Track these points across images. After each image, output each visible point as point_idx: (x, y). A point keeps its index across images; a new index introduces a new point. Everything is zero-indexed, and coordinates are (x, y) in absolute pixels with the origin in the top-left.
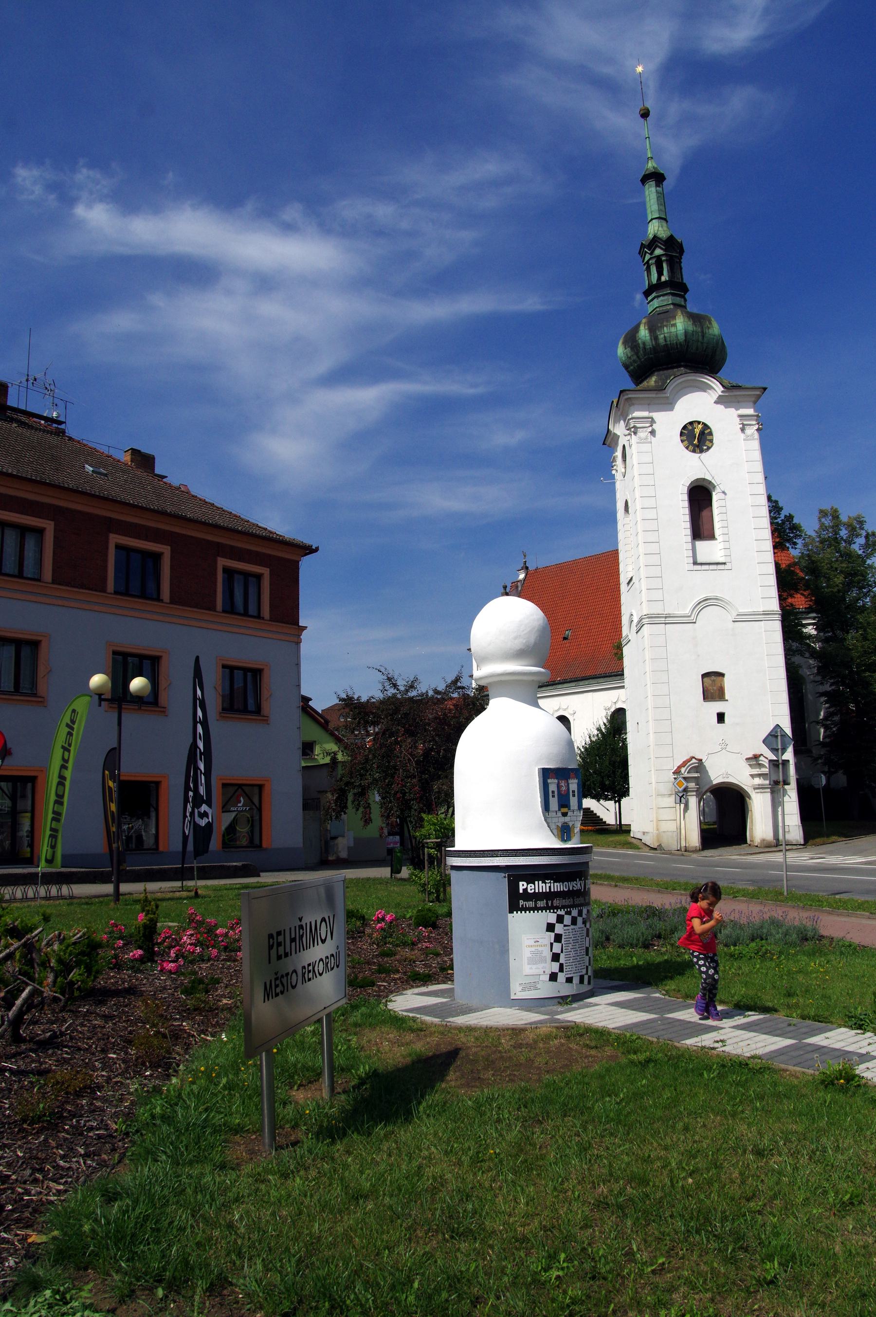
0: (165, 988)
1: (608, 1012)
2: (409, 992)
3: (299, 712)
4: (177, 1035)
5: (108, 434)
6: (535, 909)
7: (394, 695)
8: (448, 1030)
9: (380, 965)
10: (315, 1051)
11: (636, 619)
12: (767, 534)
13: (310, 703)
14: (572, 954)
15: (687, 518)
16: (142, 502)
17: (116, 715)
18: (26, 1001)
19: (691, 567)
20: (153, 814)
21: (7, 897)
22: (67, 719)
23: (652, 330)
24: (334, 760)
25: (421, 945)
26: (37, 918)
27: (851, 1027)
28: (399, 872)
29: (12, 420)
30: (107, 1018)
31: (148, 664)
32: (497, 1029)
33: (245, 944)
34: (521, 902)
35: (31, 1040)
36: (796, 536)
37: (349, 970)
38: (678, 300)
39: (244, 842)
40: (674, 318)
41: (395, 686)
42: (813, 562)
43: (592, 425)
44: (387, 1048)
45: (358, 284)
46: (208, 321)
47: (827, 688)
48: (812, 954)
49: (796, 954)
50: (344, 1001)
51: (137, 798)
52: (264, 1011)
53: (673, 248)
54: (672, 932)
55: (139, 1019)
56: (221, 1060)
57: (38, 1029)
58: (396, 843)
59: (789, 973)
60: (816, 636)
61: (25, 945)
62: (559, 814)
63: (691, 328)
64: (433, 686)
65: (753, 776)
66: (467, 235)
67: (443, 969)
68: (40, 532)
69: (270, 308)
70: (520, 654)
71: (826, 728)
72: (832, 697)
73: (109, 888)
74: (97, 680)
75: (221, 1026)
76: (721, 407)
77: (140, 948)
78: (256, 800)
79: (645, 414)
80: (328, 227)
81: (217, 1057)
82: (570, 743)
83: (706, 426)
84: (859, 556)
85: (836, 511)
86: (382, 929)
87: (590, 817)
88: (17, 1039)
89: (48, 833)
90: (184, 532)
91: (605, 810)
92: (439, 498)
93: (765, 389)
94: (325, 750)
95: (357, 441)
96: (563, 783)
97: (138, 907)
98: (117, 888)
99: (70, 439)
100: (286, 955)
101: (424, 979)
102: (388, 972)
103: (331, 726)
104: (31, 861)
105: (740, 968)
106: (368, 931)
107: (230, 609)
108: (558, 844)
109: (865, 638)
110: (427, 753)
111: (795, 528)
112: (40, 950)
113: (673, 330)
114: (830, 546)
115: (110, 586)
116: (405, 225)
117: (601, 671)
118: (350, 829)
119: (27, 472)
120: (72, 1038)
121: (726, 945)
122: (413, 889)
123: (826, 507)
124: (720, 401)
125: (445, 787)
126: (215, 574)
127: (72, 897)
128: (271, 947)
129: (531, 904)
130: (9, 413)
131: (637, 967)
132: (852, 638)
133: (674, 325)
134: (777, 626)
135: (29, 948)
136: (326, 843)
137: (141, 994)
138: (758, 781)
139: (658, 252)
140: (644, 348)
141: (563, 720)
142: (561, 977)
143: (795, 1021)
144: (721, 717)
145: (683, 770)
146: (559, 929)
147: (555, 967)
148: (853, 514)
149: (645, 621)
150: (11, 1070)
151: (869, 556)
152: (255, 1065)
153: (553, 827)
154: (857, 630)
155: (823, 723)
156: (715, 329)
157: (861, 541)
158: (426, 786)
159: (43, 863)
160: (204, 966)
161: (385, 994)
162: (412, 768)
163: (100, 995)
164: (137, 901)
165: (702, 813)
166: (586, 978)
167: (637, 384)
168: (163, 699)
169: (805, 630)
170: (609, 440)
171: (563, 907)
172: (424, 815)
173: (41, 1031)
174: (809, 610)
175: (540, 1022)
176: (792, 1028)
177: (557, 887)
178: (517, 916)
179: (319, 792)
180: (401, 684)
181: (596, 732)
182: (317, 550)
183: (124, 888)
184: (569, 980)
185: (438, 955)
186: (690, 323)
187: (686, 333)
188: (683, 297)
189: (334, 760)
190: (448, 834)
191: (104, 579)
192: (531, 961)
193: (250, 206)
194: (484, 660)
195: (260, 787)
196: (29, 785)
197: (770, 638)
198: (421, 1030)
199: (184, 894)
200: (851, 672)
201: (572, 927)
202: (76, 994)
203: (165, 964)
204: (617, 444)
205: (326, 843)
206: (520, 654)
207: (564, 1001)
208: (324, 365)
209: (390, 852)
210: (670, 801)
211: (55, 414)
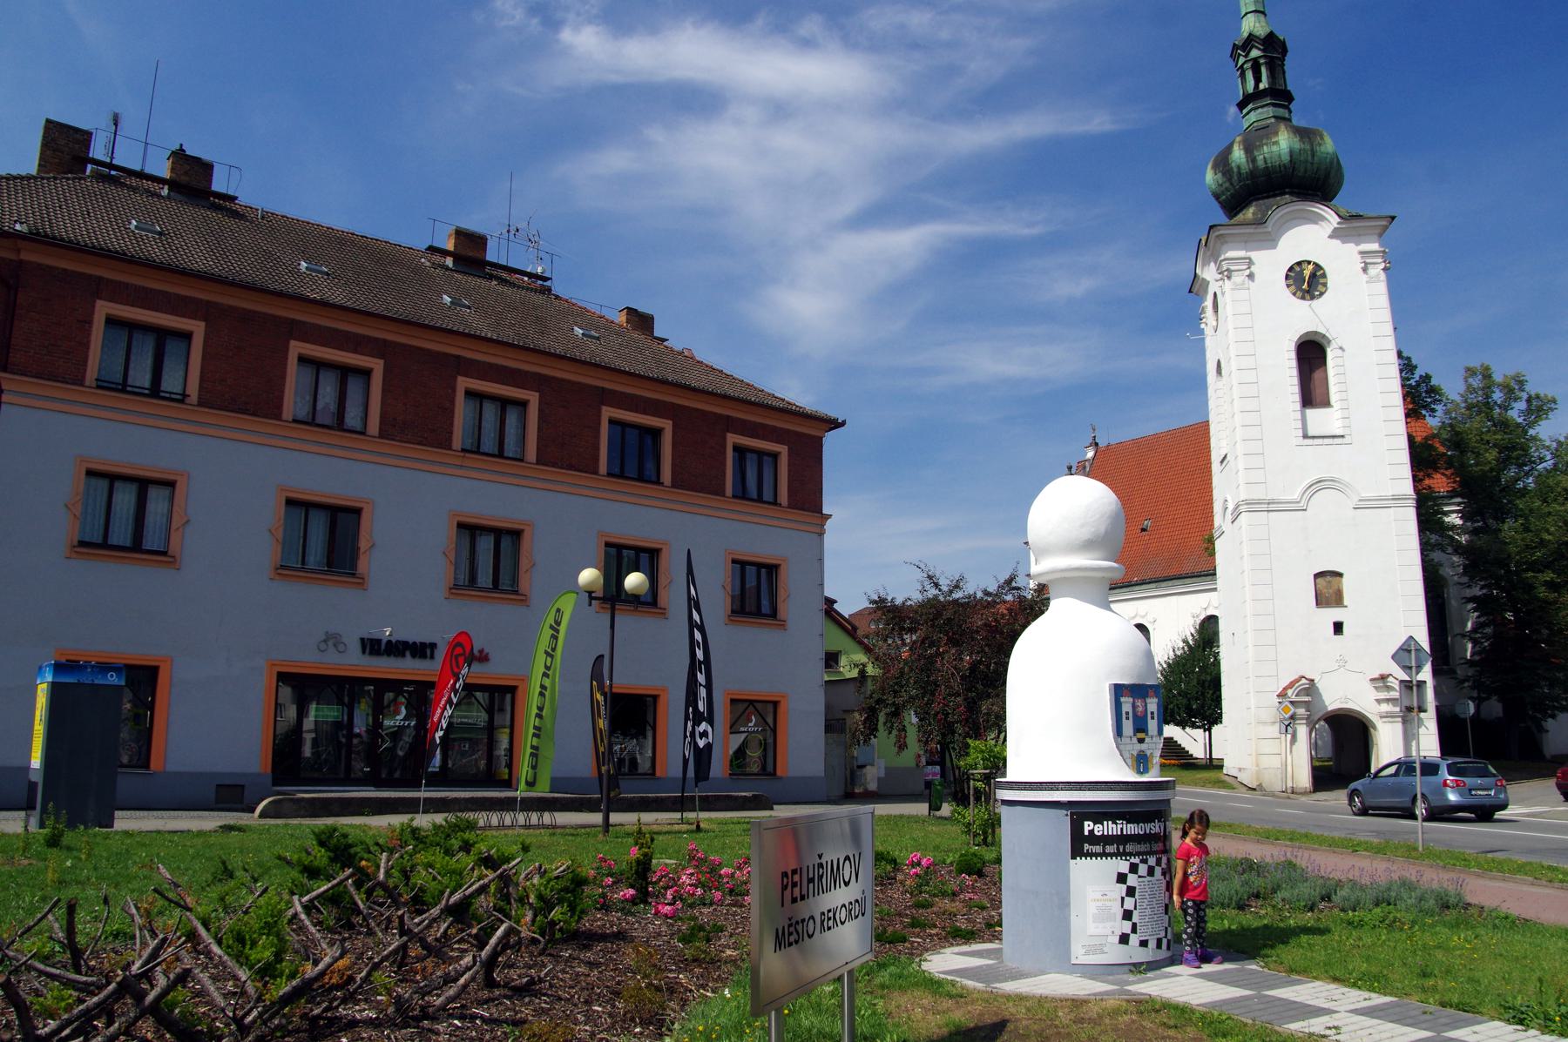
0: (659, 934)
1: (1190, 986)
2: (948, 950)
3: (821, 615)
4: (672, 989)
5: (597, 290)
6: (1104, 855)
7: (936, 596)
8: (993, 997)
9: (913, 918)
10: (834, 1015)
11: (1231, 506)
12: (1397, 399)
13: (836, 606)
14: (1148, 911)
15: (1296, 381)
16: (640, 369)
17: (607, 617)
18: (500, 940)
19: (1301, 441)
20: (650, 734)
21: (481, 823)
22: (550, 620)
23: (1249, 149)
24: (862, 673)
25: (961, 897)
26: (515, 848)
27: (1508, 1021)
28: (939, 809)
29: (491, 277)
30: (592, 965)
31: (647, 558)
32: (1054, 999)
33: (754, 887)
34: (1086, 847)
35: (506, 986)
36: (1435, 401)
37: (876, 923)
38: (1282, 112)
39: (755, 769)
40: (1276, 133)
41: (936, 585)
42: (1457, 434)
43: (1175, 268)
44: (920, 1016)
45: (887, 107)
46: (713, 156)
47: (1476, 591)
48: (1455, 926)
49: (1433, 926)
50: (870, 956)
51: (630, 714)
52: (774, 964)
53: (1274, 47)
54: (1274, 891)
55: (628, 969)
56: (722, 1020)
57: (514, 974)
58: (935, 774)
59: (1425, 946)
60: (1461, 527)
61: (501, 877)
62: (1135, 740)
63: (1297, 145)
64: (982, 586)
65: (1379, 701)
66: (1019, 45)
67: (989, 925)
68: (523, 404)
69: (786, 139)
70: (1088, 545)
71: (1475, 642)
72: (1482, 604)
73: (596, 818)
74: (588, 575)
75: (723, 981)
76: (1336, 242)
77: (632, 887)
78: (770, 720)
79: (1242, 253)
80: (851, 42)
81: (717, 1016)
82: (1149, 655)
83: (1318, 267)
84: (1518, 425)
85: (1487, 368)
86: (916, 874)
87: (1172, 750)
88: (490, 983)
89: (529, 751)
90: (687, 403)
91: (1192, 740)
92: (991, 361)
93: (1393, 218)
94: (852, 662)
95: (894, 293)
96: (1139, 703)
97: (631, 840)
98: (606, 818)
99: (557, 297)
100: (803, 898)
101: (968, 936)
102: (923, 926)
103: (860, 633)
104: (508, 784)
105: (1360, 939)
106: (900, 877)
107: (742, 494)
108: (1132, 777)
109: (1527, 529)
110: (974, 667)
111: (1433, 391)
112: (517, 884)
113: (1275, 148)
114: (1479, 413)
115: (603, 467)
116: (945, 35)
117: (1186, 570)
118: (883, 755)
119: (509, 335)
120: (551, 986)
121: (1343, 910)
122: (956, 829)
123: (1475, 363)
124: (1335, 234)
125: (995, 708)
126: (724, 453)
127: (555, 827)
128: (784, 888)
129: (1098, 849)
130: (488, 269)
131: (1229, 932)
132: (1509, 528)
133: (1276, 143)
134: (1411, 513)
135: (505, 880)
136: (853, 773)
137: (632, 939)
138: (1385, 707)
139: (1255, 53)
140: (1239, 173)
141: (1141, 628)
142: (1134, 940)
143: (1432, 1008)
144: (1338, 628)
145: (1290, 692)
146: (1132, 880)
147: (1127, 929)
148: (1511, 373)
149: (1242, 508)
150: (482, 1017)
151: (1531, 425)
152: (763, 1028)
153: (1127, 755)
154: (1516, 518)
155: (1470, 636)
156: (1328, 145)
157: (1522, 405)
158: (972, 706)
159: (522, 785)
160: (705, 910)
161: (918, 952)
162: (956, 683)
163: (585, 939)
164: (628, 835)
165: (1314, 746)
166: (1165, 941)
167: (1231, 218)
168: (662, 602)
169: (1447, 519)
170: (1196, 287)
171: (1138, 854)
172: (969, 741)
173: (517, 976)
174: (1453, 494)
175: (1107, 993)
176: (1428, 1017)
177: (1131, 829)
178: (1081, 862)
179: (845, 711)
180: (945, 584)
181: (1181, 644)
182: (843, 424)
183: (615, 818)
184: (1144, 944)
185: (983, 908)
186: (1297, 139)
187: (1291, 153)
188: (1287, 107)
189: (862, 673)
190: (997, 764)
191: (596, 459)
192: (1097, 919)
193: (760, 21)
194: (1044, 552)
195: (775, 704)
196: (509, 696)
197: (1404, 524)
198: (960, 996)
199: (685, 827)
200: (1509, 571)
202: (558, 935)
204: (1206, 291)
205: (853, 773)
206: (1088, 545)
207: (1137, 968)
208: (849, 205)
209: (928, 784)
210: (1274, 730)
211: (539, 270)
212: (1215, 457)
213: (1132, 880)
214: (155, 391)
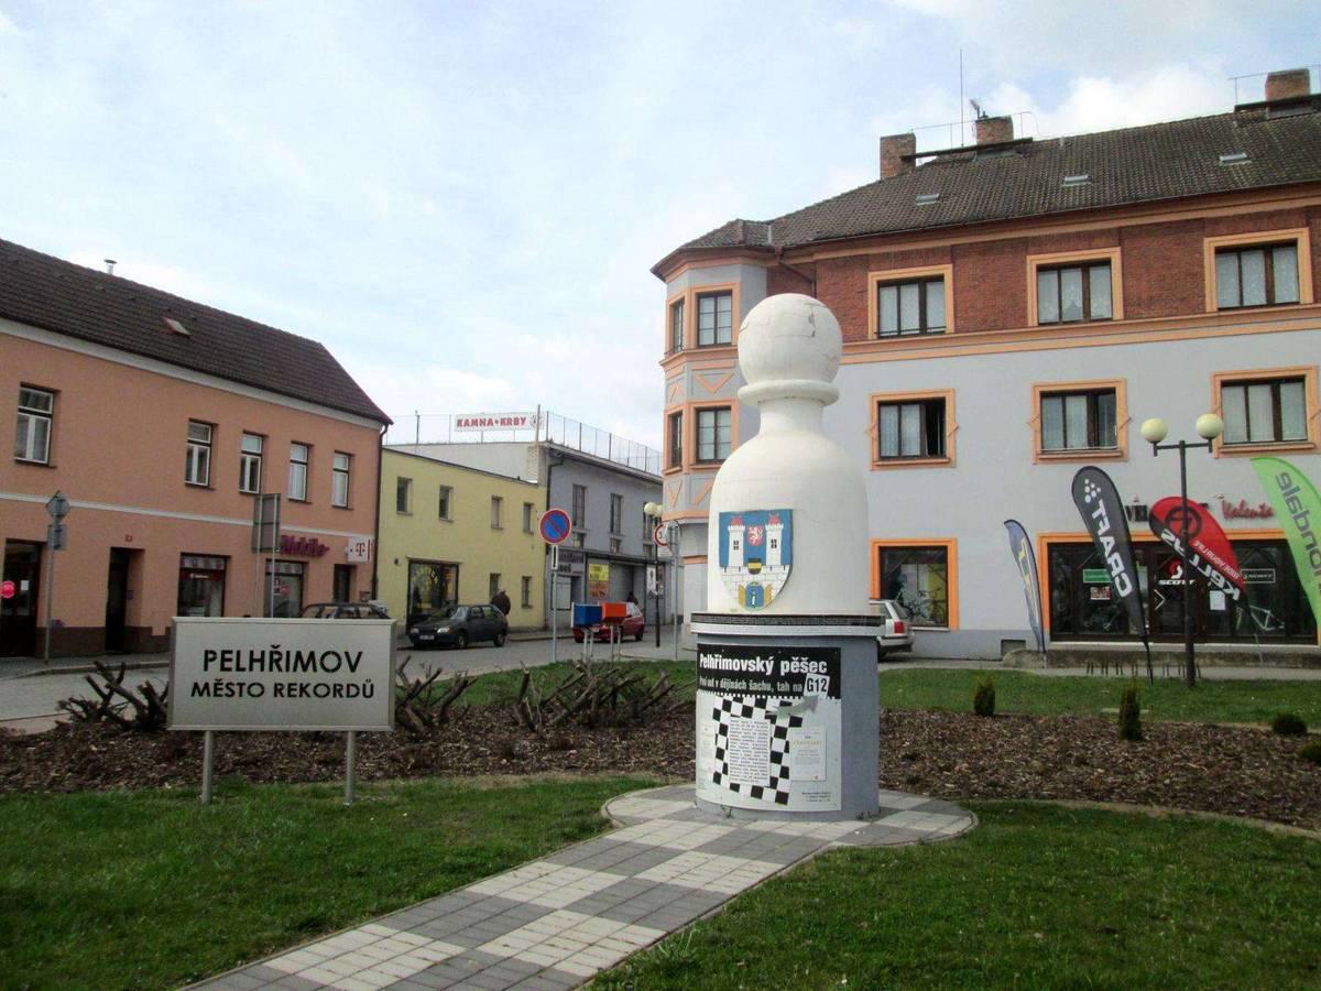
62: (745, 570)
73: (1181, 647)
171: (732, 691)
201: (745, 719)
212: (103, 268)
213: (725, 717)
214: (1271, 302)
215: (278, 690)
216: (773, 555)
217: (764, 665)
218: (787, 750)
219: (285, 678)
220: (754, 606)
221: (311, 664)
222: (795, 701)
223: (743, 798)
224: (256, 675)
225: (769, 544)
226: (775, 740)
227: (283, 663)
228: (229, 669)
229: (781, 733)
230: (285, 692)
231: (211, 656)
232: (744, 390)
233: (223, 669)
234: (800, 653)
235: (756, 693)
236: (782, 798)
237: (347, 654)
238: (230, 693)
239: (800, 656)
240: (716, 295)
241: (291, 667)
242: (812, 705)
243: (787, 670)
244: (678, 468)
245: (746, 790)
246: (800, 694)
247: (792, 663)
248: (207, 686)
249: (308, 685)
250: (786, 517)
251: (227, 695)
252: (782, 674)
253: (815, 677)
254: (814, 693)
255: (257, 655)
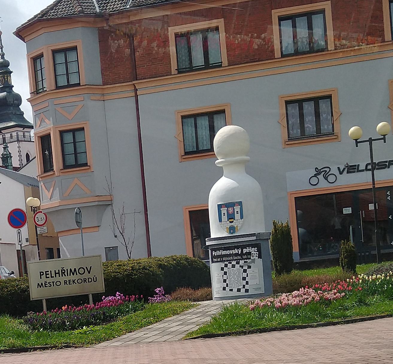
171: (227, 261)
203: (361, 280)
213: (226, 269)
215: (65, 282)
216: (238, 216)
217: (238, 251)
218: (247, 276)
219: (67, 278)
220: (232, 233)
221: (75, 273)
222: (249, 261)
223: (235, 293)
224: (58, 279)
225: (236, 213)
226: (243, 273)
227: (66, 273)
228: (49, 277)
229: (245, 271)
230: (68, 283)
231: (42, 274)
232: (217, 161)
233: (46, 277)
234: (249, 246)
235: (236, 260)
236: (247, 291)
237: (86, 268)
238: (50, 285)
239: (249, 247)
240: (65, 51)
241: (69, 275)
242: (253, 261)
243: (245, 252)
244: (51, 173)
245: (235, 290)
246: (250, 259)
247: (247, 249)
248: (42, 284)
249: (75, 280)
250: (240, 203)
251: (49, 286)
252: (244, 253)
253: (254, 253)
254: (254, 258)
255: (57, 272)
